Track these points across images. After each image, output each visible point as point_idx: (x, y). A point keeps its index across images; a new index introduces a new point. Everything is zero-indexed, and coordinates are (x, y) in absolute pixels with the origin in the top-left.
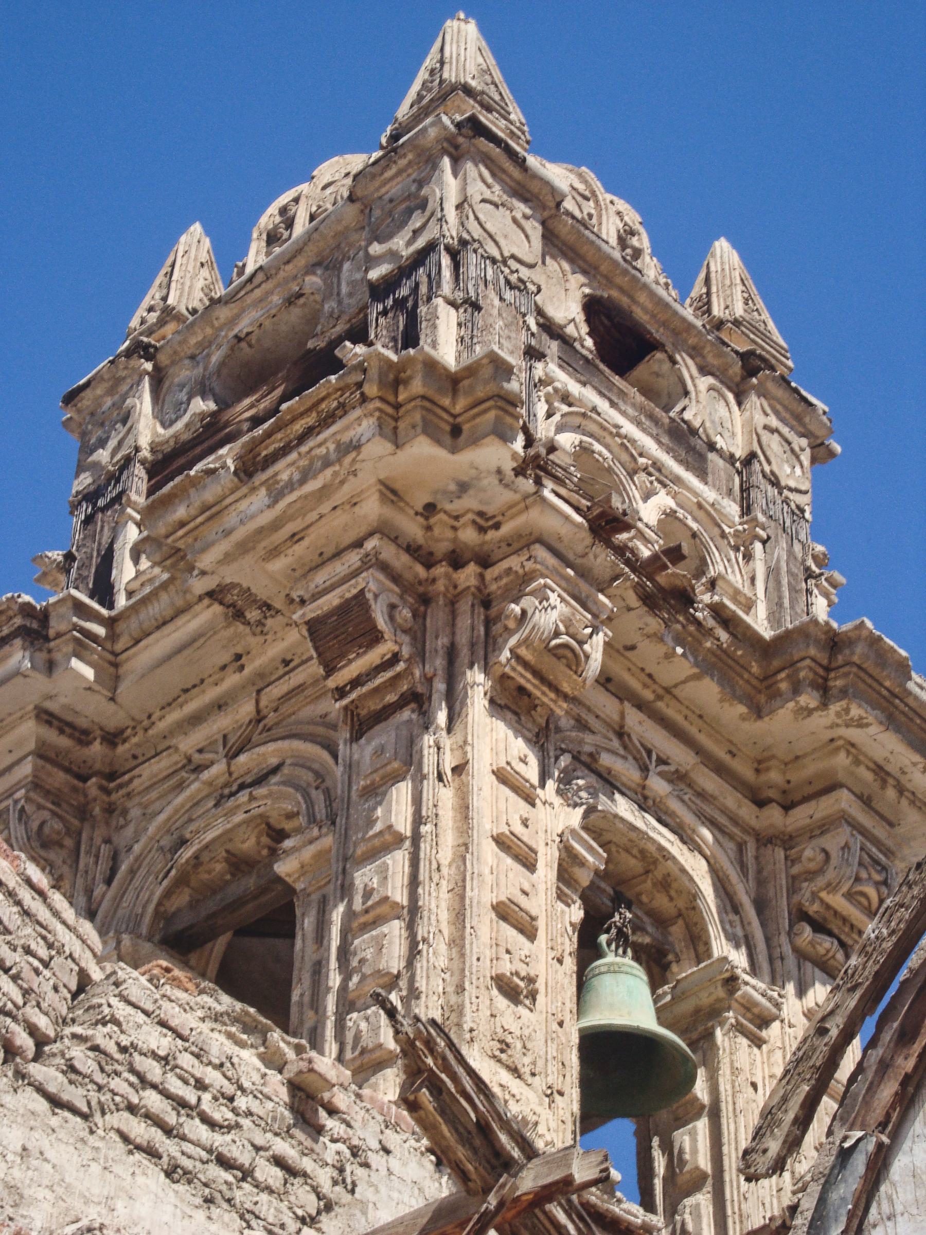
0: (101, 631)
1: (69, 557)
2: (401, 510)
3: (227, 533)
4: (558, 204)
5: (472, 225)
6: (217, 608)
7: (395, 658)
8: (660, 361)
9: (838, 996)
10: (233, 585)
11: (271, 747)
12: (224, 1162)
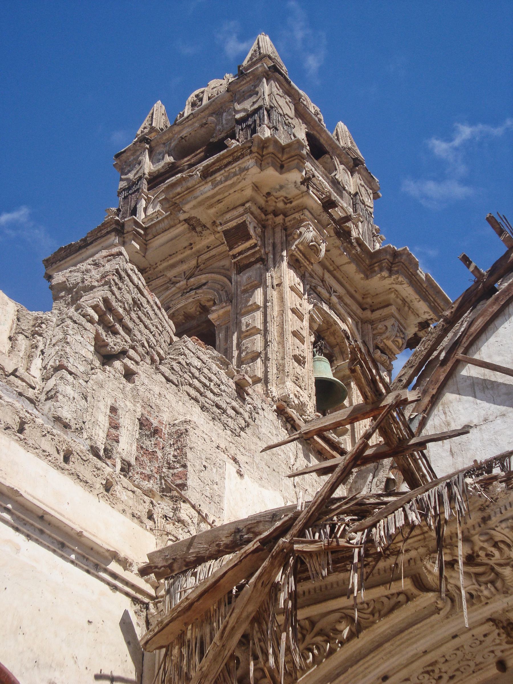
0: (142, 232)
1: (119, 210)
2: (259, 194)
3: (196, 198)
4: (300, 99)
5: (274, 102)
6: (186, 225)
7: (256, 245)
8: (328, 158)
9: (406, 370)
10: (194, 217)
11: (204, 276)
12: (218, 407)
